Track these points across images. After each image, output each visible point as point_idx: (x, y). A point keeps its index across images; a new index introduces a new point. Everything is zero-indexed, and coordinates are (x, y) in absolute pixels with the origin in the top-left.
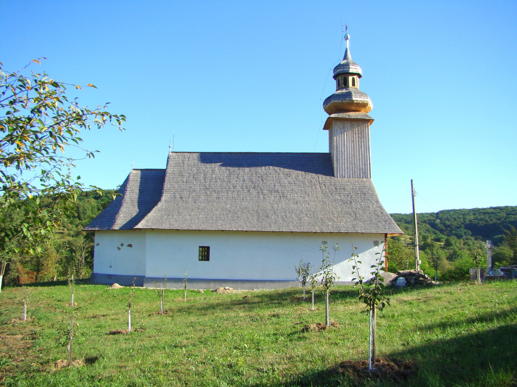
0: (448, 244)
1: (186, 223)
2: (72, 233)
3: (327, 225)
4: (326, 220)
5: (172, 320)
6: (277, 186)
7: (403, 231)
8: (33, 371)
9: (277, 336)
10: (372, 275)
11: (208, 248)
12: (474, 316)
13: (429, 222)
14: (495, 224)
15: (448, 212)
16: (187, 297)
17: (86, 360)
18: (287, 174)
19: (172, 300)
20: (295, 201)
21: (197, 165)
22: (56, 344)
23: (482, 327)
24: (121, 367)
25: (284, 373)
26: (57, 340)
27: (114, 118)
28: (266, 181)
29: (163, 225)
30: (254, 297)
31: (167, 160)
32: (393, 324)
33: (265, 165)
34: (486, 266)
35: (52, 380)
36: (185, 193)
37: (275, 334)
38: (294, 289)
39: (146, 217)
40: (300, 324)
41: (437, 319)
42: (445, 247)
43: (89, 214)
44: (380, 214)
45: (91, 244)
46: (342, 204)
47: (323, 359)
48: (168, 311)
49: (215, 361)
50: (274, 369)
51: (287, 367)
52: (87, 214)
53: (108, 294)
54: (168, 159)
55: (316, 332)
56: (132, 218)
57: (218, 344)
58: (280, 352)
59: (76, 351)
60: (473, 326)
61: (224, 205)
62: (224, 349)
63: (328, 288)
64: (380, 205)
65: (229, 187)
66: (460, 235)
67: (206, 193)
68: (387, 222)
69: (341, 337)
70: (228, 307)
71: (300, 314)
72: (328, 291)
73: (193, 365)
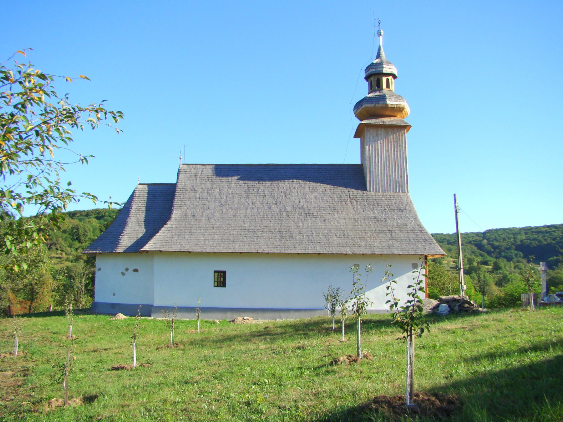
0: (497, 268)
1: (199, 244)
2: (71, 257)
3: (359, 246)
4: (358, 240)
5: (183, 354)
6: (302, 202)
7: (446, 253)
8: (24, 412)
9: (302, 370)
10: (409, 296)
11: (224, 273)
12: (527, 346)
13: (475, 242)
14: (549, 245)
15: (497, 231)
16: (201, 328)
17: (84, 399)
18: (313, 188)
19: (184, 331)
20: (323, 219)
21: (211, 178)
22: (50, 382)
23: (536, 356)
24: (123, 406)
25: (310, 410)
26: (52, 377)
27: (109, 115)
28: (289, 196)
29: (173, 247)
30: (277, 327)
31: (178, 174)
32: (435, 355)
33: (289, 179)
34: (540, 291)
35: (45, 421)
36: (198, 210)
37: (300, 368)
38: (322, 318)
39: (154, 238)
40: (328, 356)
41: (484, 349)
42: (493, 270)
43: (91, 236)
44: (419, 232)
45: (92, 269)
46: (376, 222)
47: (354, 394)
48: (179, 343)
49: (230, 398)
50: (298, 406)
51: (312, 404)
52: (88, 237)
53: (111, 325)
54: (178, 172)
55: (346, 365)
56: (138, 239)
57: (234, 379)
58: (305, 388)
59: (73, 388)
60: (526, 356)
61: (242, 224)
62: (241, 385)
63: (359, 315)
64: (419, 223)
65: (248, 203)
66: (510, 257)
67: (222, 210)
68: (428, 242)
69: (375, 371)
70: (246, 338)
71: (328, 346)
72: (360, 318)
73: (205, 403)
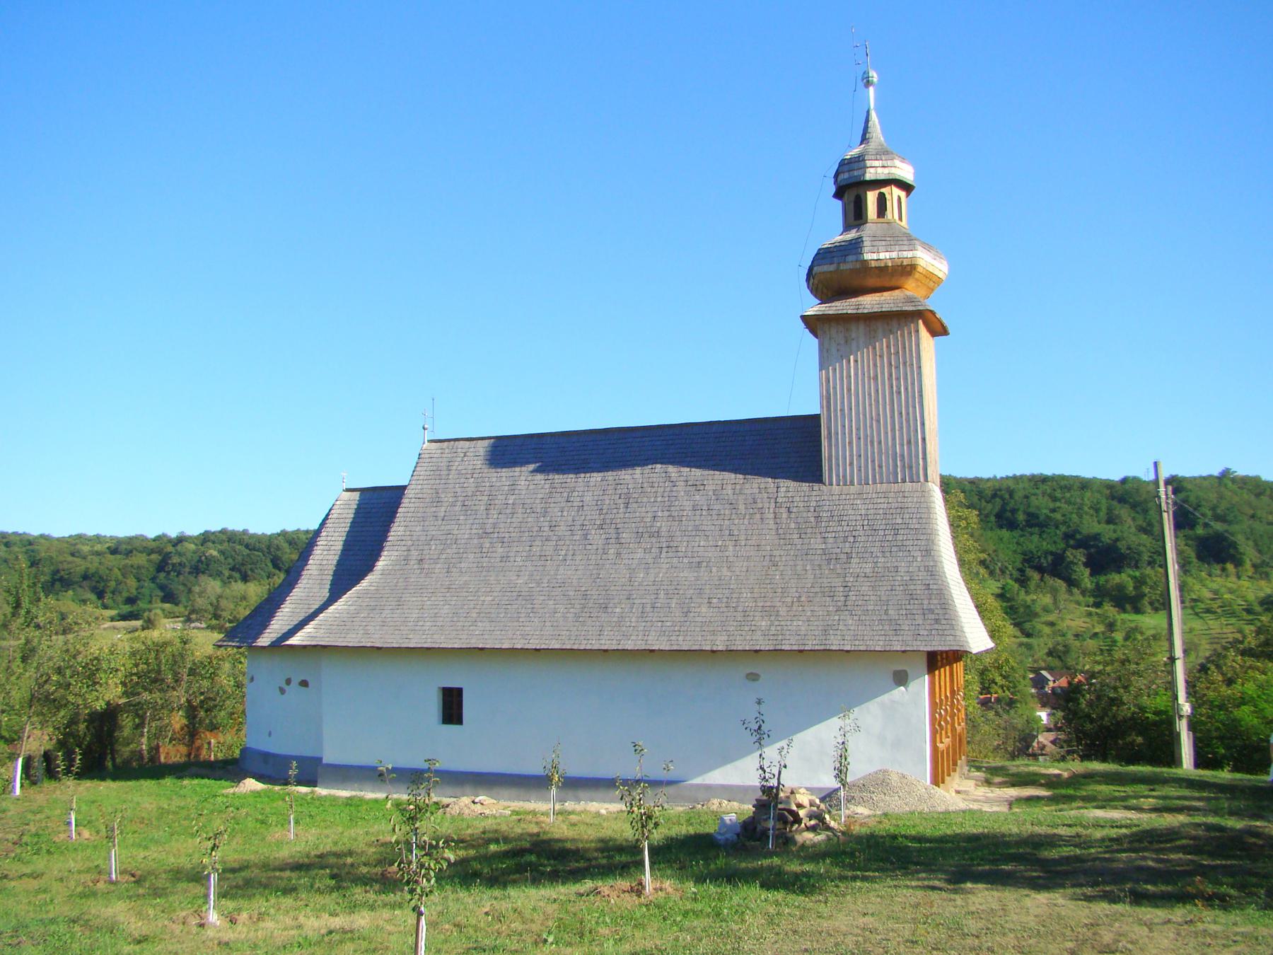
3: (753, 628)
36: (433, 548)
